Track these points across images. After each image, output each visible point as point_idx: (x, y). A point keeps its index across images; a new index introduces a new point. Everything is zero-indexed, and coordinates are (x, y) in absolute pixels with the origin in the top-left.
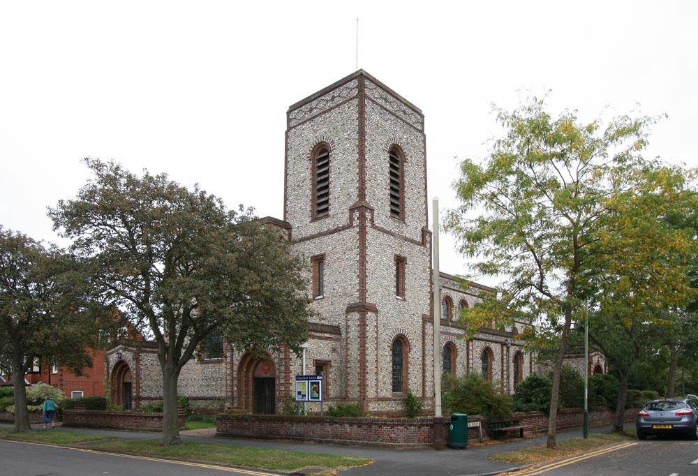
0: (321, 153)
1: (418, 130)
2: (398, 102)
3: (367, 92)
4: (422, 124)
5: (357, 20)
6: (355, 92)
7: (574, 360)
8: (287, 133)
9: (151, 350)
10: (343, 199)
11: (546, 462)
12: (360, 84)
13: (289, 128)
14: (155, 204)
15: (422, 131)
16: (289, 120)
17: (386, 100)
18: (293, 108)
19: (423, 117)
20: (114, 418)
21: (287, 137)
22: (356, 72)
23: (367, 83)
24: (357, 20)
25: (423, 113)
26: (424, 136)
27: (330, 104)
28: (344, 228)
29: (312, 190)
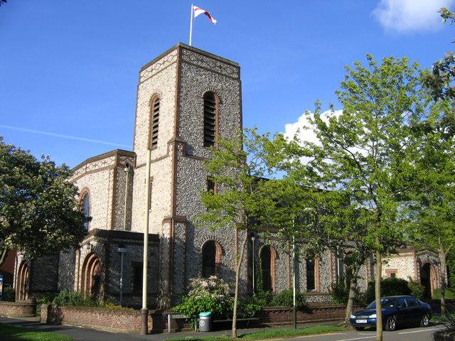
1: (234, 79)
2: (208, 59)
4: (239, 73)
6: (176, 58)
7: (403, 259)
10: (165, 134)
14: (446, 151)
15: (238, 79)
17: (202, 61)
27: (162, 67)
28: (165, 157)
29: (150, 128)
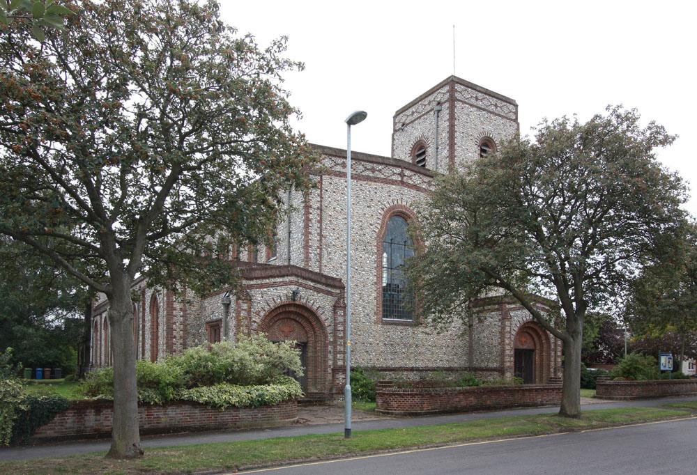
0: (420, 149)
3: (458, 95)
4: (516, 113)
5: (454, 26)
8: (393, 135)
9: (259, 282)
11: (394, 450)
12: (453, 90)
13: (395, 131)
16: (395, 124)
18: (398, 113)
19: (516, 106)
20: (527, 393)
21: (393, 139)
22: (447, 79)
23: (458, 87)
24: (454, 26)
25: (517, 102)
26: (518, 124)
